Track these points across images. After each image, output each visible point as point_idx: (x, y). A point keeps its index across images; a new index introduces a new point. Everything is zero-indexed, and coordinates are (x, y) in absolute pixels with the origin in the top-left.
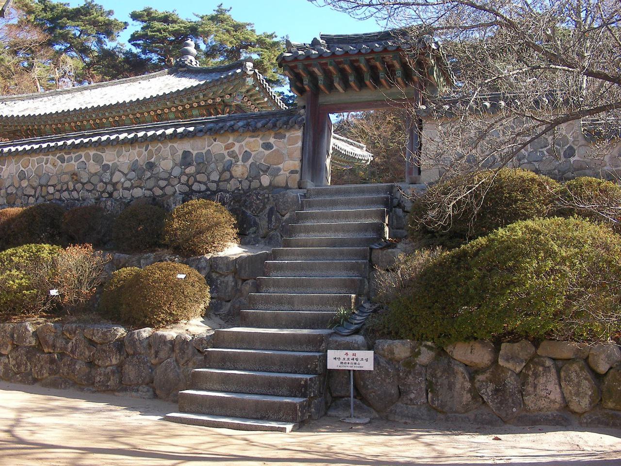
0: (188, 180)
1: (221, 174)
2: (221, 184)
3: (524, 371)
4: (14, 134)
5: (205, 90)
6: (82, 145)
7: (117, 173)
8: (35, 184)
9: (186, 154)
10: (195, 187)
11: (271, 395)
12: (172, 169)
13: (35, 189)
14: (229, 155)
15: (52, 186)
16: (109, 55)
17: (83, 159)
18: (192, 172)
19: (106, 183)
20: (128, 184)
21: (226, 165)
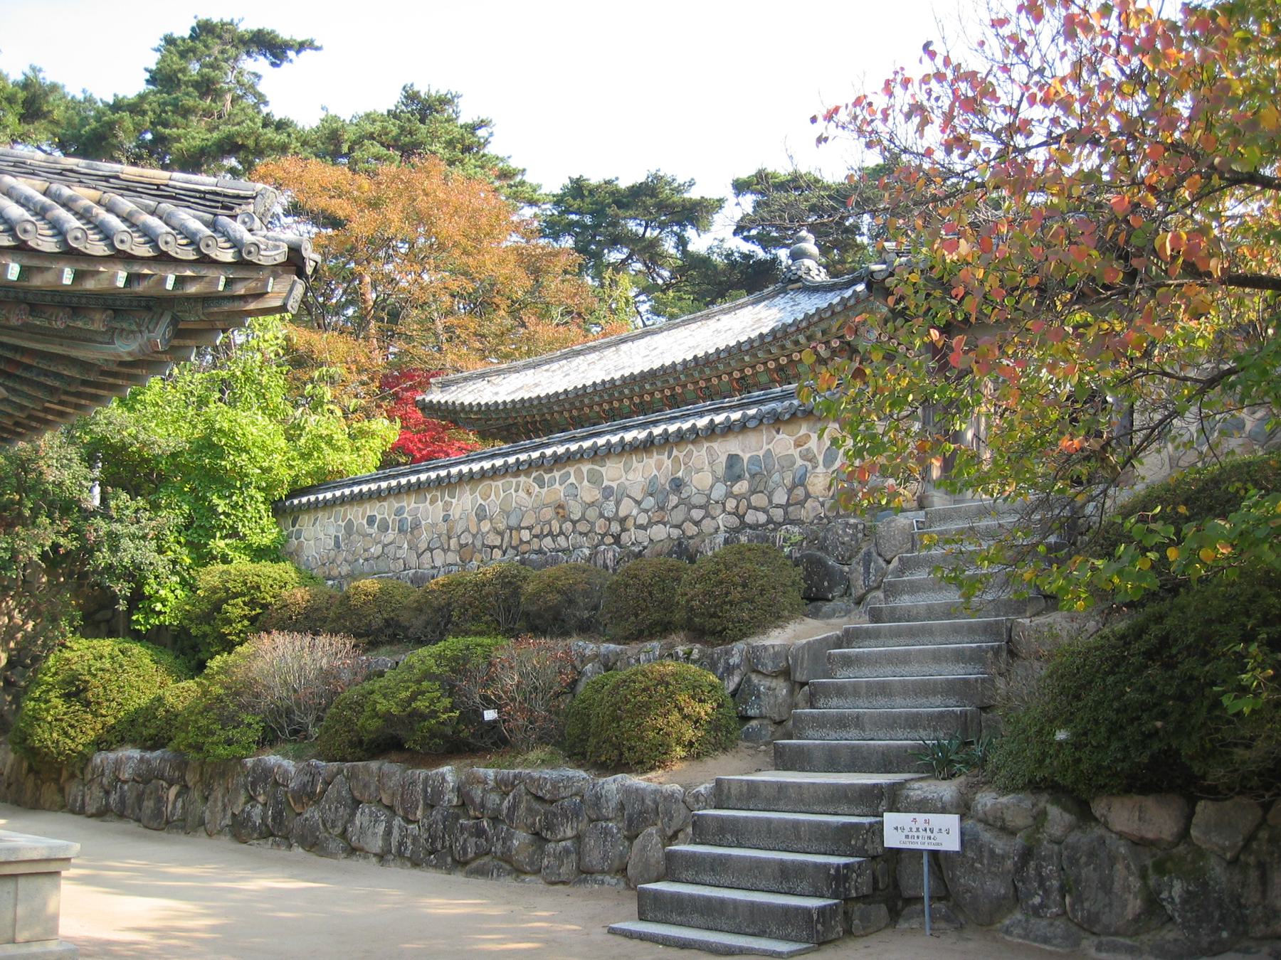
0: (737, 507)
1: (790, 491)
2: (791, 509)
3: (1242, 857)
4: (508, 430)
5: (808, 328)
6: (569, 458)
7: (626, 500)
8: (501, 527)
9: (733, 460)
10: (750, 518)
11: (786, 893)
12: (712, 487)
13: (501, 534)
14: (803, 457)
15: (527, 528)
16: (694, 265)
17: (572, 480)
18: (743, 490)
19: (609, 520)
20: (643, 519)
21: (798, 476)
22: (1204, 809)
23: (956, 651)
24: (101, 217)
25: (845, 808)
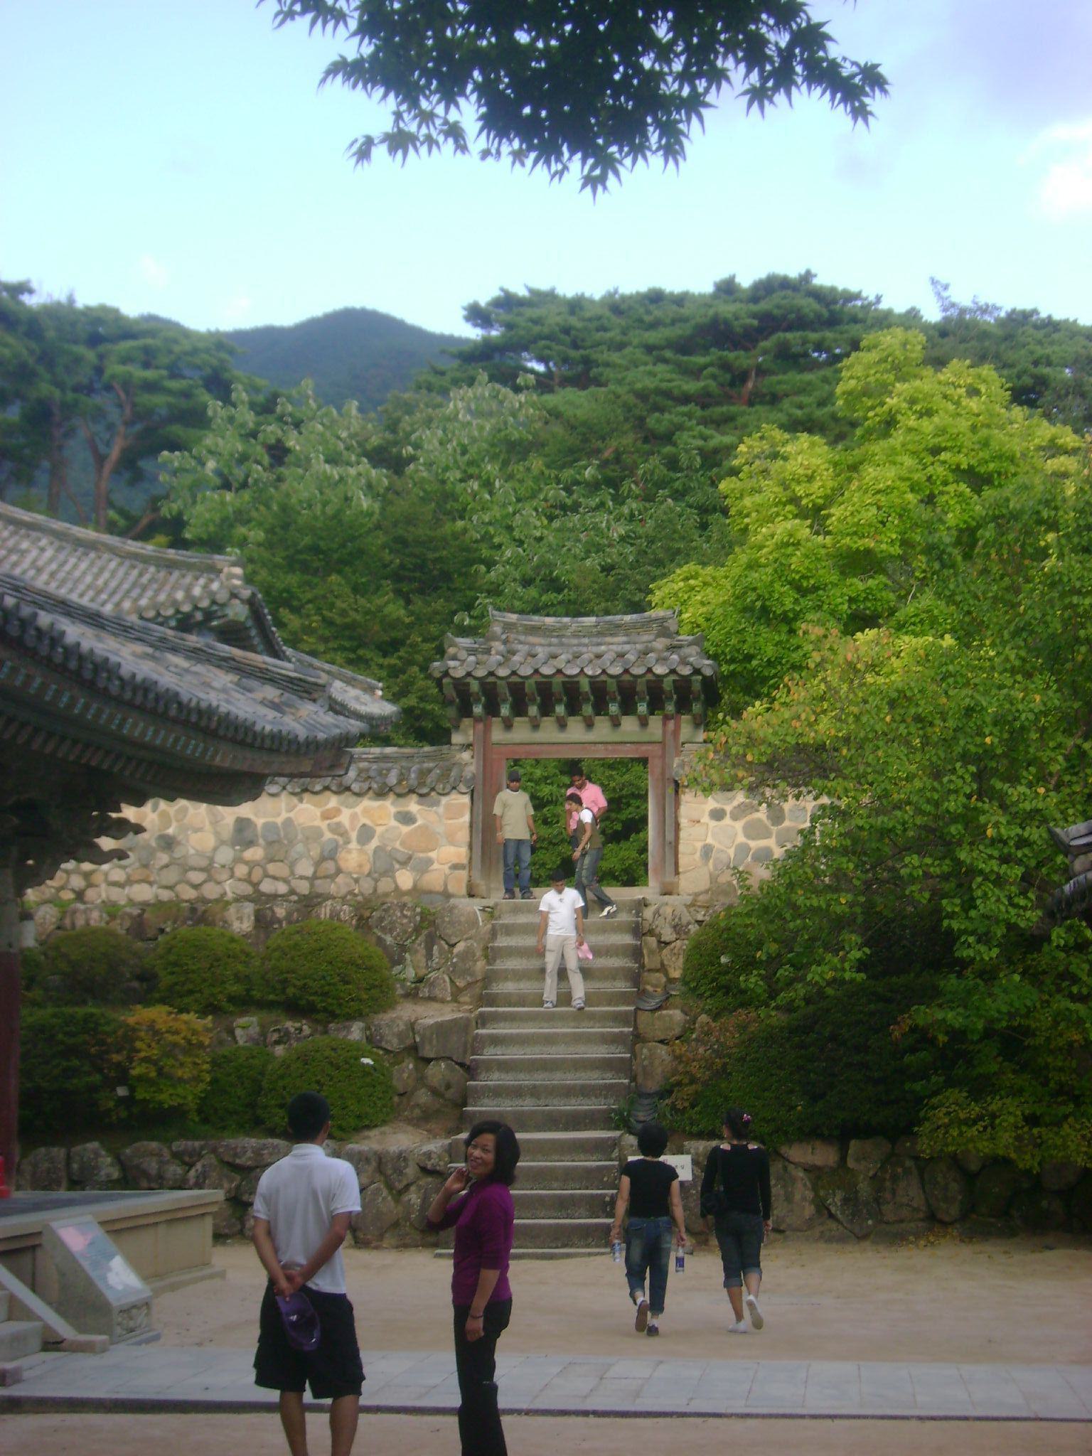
0: (250, 874)
1: (318, 864)
2: (318, 882)
22: (854, 1145)
23: (602, 1034)
24: (86, 645)
25: (582, 1157)
